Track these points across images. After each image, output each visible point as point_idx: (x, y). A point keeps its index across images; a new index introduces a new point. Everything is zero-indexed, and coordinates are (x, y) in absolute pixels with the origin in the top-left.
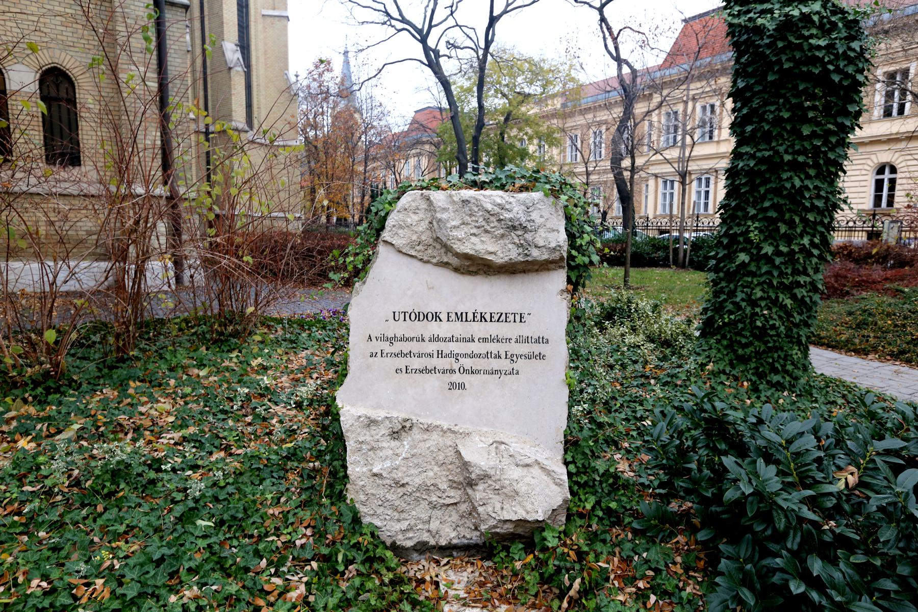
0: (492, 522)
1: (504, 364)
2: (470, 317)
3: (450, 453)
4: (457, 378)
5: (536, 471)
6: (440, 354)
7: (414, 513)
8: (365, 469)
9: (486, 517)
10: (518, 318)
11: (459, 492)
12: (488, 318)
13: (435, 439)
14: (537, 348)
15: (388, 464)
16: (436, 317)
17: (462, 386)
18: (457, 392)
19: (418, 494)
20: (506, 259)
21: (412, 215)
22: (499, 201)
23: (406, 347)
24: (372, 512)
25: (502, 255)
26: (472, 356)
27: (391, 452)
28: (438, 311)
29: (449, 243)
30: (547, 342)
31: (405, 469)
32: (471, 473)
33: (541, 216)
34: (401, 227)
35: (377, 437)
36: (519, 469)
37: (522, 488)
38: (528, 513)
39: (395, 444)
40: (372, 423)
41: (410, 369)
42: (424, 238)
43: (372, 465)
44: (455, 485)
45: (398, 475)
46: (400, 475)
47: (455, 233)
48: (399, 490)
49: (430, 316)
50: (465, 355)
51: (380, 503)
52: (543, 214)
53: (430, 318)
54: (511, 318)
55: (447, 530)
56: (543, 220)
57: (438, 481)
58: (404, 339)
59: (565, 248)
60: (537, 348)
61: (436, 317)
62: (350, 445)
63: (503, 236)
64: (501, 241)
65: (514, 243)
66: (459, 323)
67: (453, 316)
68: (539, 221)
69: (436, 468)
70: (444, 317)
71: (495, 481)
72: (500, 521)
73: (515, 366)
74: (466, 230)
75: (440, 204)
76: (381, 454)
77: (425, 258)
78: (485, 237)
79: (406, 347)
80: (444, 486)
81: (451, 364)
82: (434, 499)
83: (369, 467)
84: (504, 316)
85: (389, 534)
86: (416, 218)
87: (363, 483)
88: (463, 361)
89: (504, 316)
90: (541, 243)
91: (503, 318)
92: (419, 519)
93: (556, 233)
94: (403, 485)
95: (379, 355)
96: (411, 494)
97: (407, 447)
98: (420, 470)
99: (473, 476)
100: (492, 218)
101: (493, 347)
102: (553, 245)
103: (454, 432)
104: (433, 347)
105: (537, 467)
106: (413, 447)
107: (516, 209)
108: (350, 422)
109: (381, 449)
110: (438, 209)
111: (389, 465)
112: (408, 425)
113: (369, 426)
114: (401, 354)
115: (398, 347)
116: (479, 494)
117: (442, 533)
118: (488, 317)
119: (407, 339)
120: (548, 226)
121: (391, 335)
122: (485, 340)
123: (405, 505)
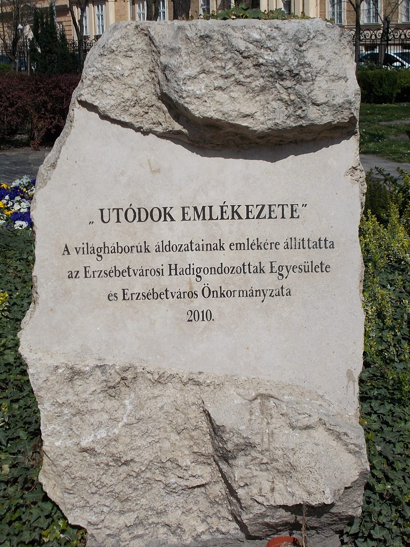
0: (257, 510)
1: (268, 281)
2: (217, 212)
3: (195, 414)
4: (200, 304)
5: (320, 434)
6: (173, 269)
7: (143, 501)
8: (69, 443)
9: (250, 502)
10: (287, 211)
11: (209, 469)
12: (243, 214)
13: (171, 393)
14: (317, 256)
15: (102, 433)
16: (166, 214)
17: (207, 316)
18: (201, 324)
19: (149, 475)
20: (270, 124)
21: (122, 60)
22: (256, 35)
23: (121, 261)
24: (82, 503)
25: (262, 119)
26: (221, 270)
27: (106, 416)
28: (169, 206)
29: (181, 101)
30: (332, 246)
31: (128, 440)
32: (226, 442)
33: (321, 57)
34: (106, 80)
35: (85, 396)
36: (297, 433)
37: (301, 460)
38: (310, 494)
39: (110, 404)
40: (75, 374)
41: (129, 293)
42: (142, 95)
43: (78, 436)
44: (202, 459)
45: (119, 448)
46: (121, 448)
47: (190, 87)
48: (121, 470)
49: (156, 213)
50: (212, 270)
51: (94, 489)
52: (324, 53)
53: (156, 217)
54: (278, 211)
55: (193, 523)
56: (323, 63)
57: (177, 454)
58: (118, 249)
59: (358, 105)
60: (317, 256)
61: (166, 214)
62: (45, 409)
63: (263, 89)
64: (261, 97)
65: (281, 100)
66: (199, 222)
67: (191, 212)
68: (319, 64)
69: (174, 437)
70: (176, 213)
71: (261, 452)
72: (271, 507)
73: (284, 283)
74: (207, 81)
75: (166, 42)
76: (92, 420)
77: (146, 126)
78: (237, 92)
79: (121, 261)
80: (186, 461)
81: (190, 283)
82: (173, 480)
83: (75, 440)
84: (266, 209)
85: (108, 532)
86: (128, 63)
87: (66, 463)
88: (207, 278)
89: (266, 209)
90: (321, 99)
91: (265, 212)
92: (152, 509)
93: (342, 82)
94: (126, 463)
95: (82, 274)
96: (138, 474)
97: (129, 407)
98: (150, 440)
99: (230, 446)
100: (248, 63)
101: (252, 257)
102: (339, 100)
103: (198, 384)
104: (161, 260)
105: (321, 429)
106: (139, 406)
107: (282, 49)
108: (43, 376)
109: (91, 412)
110: (163, 51)
111: (104, 435)
112: (129, 375)
113: (71, 380)
114: (115, 272)
115: (110, 261)
116: (239, 471)
117: (184, 527)
118: (242, 212)
119: (123, 250)
120: (331, 72)
121: (97, 244)
122: (239, 246)
123: (130, 490)
